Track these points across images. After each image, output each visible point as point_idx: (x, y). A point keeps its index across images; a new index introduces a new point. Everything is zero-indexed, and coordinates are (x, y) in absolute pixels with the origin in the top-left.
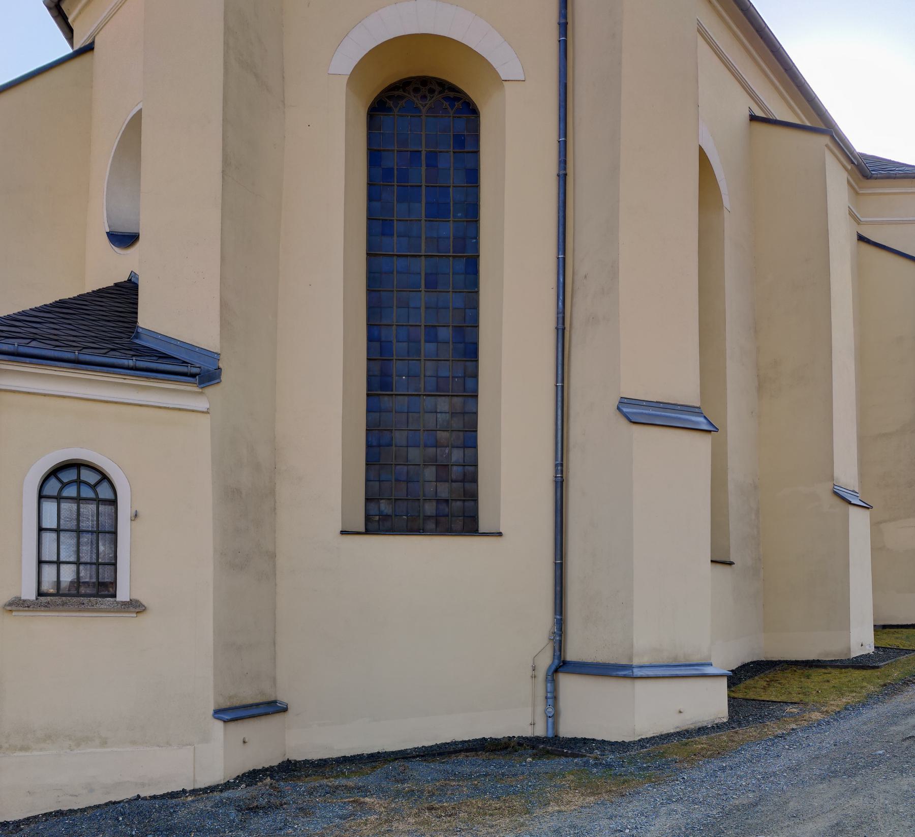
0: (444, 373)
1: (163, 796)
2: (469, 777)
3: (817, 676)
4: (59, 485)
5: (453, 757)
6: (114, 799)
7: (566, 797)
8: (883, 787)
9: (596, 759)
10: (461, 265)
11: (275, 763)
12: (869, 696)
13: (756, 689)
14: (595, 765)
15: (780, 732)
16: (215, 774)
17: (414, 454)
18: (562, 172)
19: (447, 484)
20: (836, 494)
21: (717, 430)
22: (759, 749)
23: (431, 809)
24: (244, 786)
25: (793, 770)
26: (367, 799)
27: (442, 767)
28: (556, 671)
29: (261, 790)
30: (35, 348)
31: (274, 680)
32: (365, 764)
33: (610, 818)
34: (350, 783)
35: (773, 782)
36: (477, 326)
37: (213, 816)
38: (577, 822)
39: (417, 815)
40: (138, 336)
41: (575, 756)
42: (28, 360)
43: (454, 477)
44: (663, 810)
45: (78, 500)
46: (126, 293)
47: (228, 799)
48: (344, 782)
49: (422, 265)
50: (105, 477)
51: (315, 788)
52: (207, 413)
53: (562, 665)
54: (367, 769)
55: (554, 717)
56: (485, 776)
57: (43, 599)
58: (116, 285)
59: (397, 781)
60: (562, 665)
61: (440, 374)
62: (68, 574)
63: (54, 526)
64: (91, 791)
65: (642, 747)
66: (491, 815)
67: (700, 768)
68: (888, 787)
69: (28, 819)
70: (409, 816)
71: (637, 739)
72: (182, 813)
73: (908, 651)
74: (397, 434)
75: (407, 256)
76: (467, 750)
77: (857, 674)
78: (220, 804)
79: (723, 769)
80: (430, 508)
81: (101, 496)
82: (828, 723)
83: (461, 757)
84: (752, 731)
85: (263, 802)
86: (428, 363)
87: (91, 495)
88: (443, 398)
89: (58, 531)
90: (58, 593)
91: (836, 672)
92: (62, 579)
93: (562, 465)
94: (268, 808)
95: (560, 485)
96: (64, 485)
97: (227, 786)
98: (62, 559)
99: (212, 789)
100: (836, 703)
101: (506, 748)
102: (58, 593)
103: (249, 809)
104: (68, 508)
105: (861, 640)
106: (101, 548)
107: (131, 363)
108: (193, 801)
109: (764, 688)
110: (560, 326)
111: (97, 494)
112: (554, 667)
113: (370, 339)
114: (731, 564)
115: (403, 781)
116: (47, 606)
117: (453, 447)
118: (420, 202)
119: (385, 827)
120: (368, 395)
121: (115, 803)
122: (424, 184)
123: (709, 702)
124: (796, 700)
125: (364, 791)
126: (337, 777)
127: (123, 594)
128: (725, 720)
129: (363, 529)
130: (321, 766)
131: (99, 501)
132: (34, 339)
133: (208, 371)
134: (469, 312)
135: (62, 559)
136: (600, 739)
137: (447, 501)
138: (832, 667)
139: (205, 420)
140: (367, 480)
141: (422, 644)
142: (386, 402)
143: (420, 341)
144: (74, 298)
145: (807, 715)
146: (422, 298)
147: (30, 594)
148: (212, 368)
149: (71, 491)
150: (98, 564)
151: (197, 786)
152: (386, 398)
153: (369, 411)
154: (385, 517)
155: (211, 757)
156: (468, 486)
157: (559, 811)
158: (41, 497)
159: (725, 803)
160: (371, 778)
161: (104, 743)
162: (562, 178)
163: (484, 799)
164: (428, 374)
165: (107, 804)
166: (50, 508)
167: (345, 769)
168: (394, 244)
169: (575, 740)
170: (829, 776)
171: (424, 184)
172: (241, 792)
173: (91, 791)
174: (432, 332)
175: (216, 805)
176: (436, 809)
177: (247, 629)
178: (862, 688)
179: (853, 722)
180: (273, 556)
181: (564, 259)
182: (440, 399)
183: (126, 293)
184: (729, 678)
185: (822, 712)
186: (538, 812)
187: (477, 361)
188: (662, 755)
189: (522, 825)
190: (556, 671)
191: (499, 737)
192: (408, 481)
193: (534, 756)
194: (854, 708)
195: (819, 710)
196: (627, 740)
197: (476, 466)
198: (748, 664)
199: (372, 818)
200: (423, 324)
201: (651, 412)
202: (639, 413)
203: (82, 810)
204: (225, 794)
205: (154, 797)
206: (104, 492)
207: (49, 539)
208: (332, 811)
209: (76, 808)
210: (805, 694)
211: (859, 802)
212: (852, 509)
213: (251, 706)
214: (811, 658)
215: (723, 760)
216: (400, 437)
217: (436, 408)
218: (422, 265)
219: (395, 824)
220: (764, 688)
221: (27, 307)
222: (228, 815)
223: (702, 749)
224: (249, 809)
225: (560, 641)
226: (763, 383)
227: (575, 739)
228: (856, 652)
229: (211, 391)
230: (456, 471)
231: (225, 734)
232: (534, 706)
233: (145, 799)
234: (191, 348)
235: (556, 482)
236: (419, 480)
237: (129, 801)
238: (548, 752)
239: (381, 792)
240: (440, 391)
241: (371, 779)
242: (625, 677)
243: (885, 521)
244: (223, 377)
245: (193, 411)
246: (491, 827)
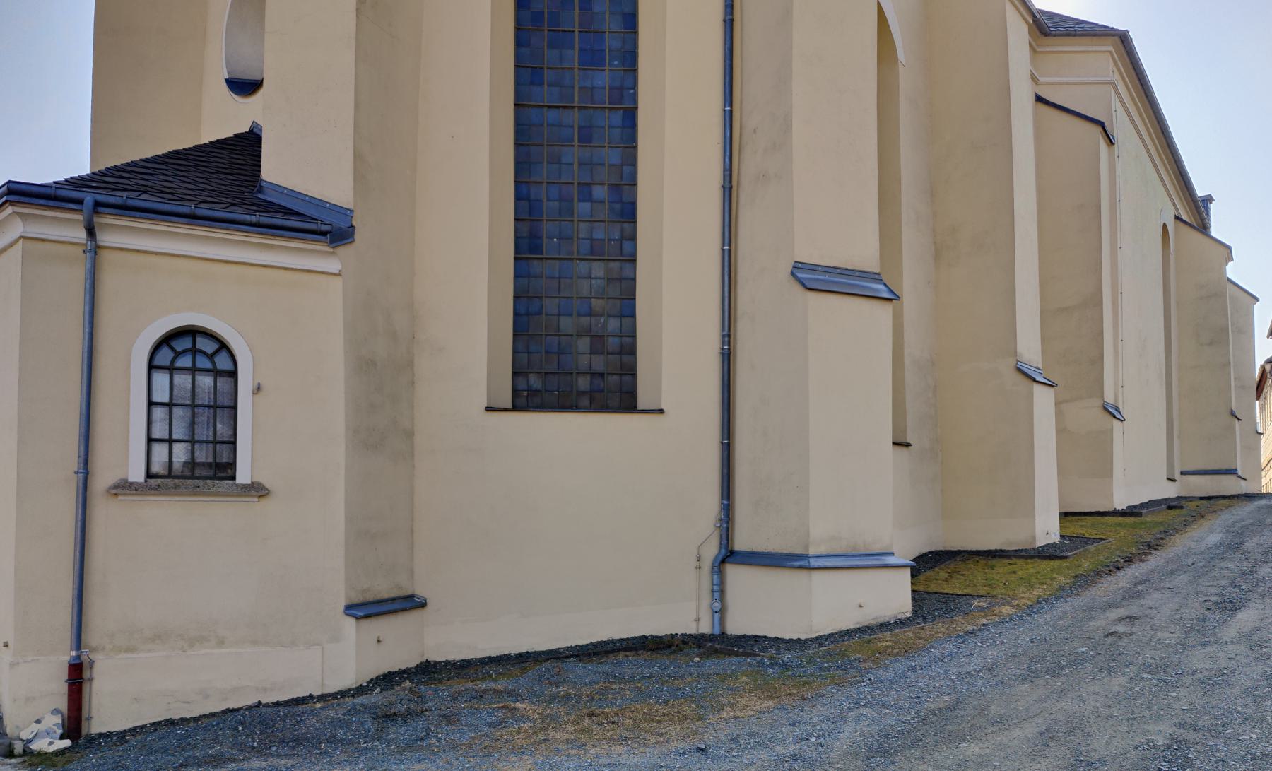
0: (599, 234)
1: (287, 703)
2: (632, 679)
3: (1002, 567)
4: (171, 355)
5: (612, 658)
6: (231, 707)
7: (745, 701)
8: (1092, 688)
9: (771, 658)
10: (617, 118)
11: (413, 664)
12: (1061, 588)
13: (938, 580)
14: (771, 665)
15: (970, 628)
16: (347, 678)
17: (566, 324)
18: (729, 17)
19: (602, 357)
20: (1019, 370)
21: (898, 298)
22: (949, 647)
23: (591, 715)
24: (378, 690)
25: (990, 670)
26: (518, 705)
27: (600, 668)
28: (723, 561)
29: (399, 695)
30: (146, 201)
31: (411, 572)
32: (513, 665)
33: (793, 724)
34: (499, 687)
35: (968, 683)
36: (636, 185)
37: (345, 725)
38: (755, 729)
39: (576, 722)
40: (261, 190)
41: (747, 655)
42: (138, 214)
43: (610, 349)
44: (851, 715)
45: (193, 370)
46: (249, 143)
47: (362, 705)
48: (492, 685)
49: (575, 118)
50: (223, 346)
51: (459, 693)
52: (339, 275)
53: (729, 556)
54: (516, 670)
55: (721, 613)
56: (649, 677)
57: (152, 482)
58: (236, 135)
59: (551, 684)
60: (729, 556)
61: (595, 236)
62: (181, 453)
63: (166, 399)
64: (207, 697)
65: (821, 645)
66: (659, 722)
67: (886, 667)
68: (1097, 689)
69: (134, 729)
70: (566, 723)
71: (814, 636)
72: (311, 721)
73: (1095, 540)
74: (547, 302)
75: (558, 107)
76: (626, 650)
77: (1045, 565)
78: (354, 711)
79: (913, 669)
80: (583, 383)
81: (220, 367)
82: (1021, 618)
83: (620, 656)
84: (940, 627)
85: (402, 708)
86: (582, 225)
87: (208, 365)
88: (598, 263)
89: (170, 405)
90: (170, 475)
91: (1021, 562)
92: (174, 459)
93: (729, 336)
94: (408, 716)
95: (727, 357)
96: (178, 354)
97: (360, 691)
98: (175, 436)
99: (342, 694)
100: (1027, 596)
101: (670, 647)
102: (170, 475)
103: (386, 716)
104: (183, 380)
105: (1047, 530)
106: (219, 426)
107: (254, 219)
108: (322, 708)
109: (946, 580)
110: (727, 185)
111: (214, 364)
112: (720, 558)
113: (518, 198)
114: (908, 445)
115: (557, 684)
116: (157, 490)
117: (609, 316)
118: (573, 48)
119: (541, 736)
120: (515, 258)
121: (233, 710)
122: (577, 29)
123: (891, 595)
124: (982, 592)
125: (514, 695)
126: (483, 679)
127: (243, 475)
128: (909, 615)
129: (510, 406)
130: (464, 668)
131: (217, 373)
132: (145, 192)
133: (340, 229)
134: (626, 169)
135: (175, 436)
136: (773, 636)
137: (602, 375)
138: (1016, 557)
139: (338, 282)
140: (515, 352)
141: (573, 532)
142: (536, 267)
143: (572, 200)
144: (190, 149)
145: (996, 610)
146: (574, 154)
147: (138, 475)
148: (344, 226)
149: (185, 361)
150: (215, 442)
151: (326, 691)
152: (535, 262)
153: (516, 276)
154: (533, 393)
155: (344, 658)
156: (626, 358)
157: (735, 718)
158: (152, 367)
159: (918, 707)
160: (522, 681)
161: (221, 643)
162: (729, 24)
163: (650, 704)
164: (581, 236)
165: (224, 712)
166: (161, 379)
167: (492, 670)
168: (545, 94)
169: (744, 638)
170: (1031, 675)
171: (577, 29)
172: (375, 698)
173: (207, 697)
174: (586, 191)
175: (349, 713)
176: (597, 715)
177: (378, 521)
178: (1052, 579)
179: (1048, 617)
180: (410, 434)
181: (731, 111)
182: (595, 264)
183: (249, 143)
184: (912, 568)
185: (1013, 606)
186: (712, 718)
187: (635, 222)
188: (843, 654)
189: (696, 733)
190: (723, 561)
191: (661, 634)
192: (559, 353)
193: (701, 656)
194: (1047, 601)
195: (1009, 604)
196: (803, 637)
197: (634, 336)
198: (926, 554)
199: (526, 726)
200: (576, 182)
201: (827, 277)
202: (815, 279)
203: (196, 719)
204: (359, 700)
205: (277, 704)
206: (222, 362)
207: (159, 413)
208: (480, 719)
209: (188, 716)
210: (991, 586)
211: (1067, 704)
212: (1037, 387)
213: (386, 601)
214: (993, 548)
215: (912, 658)
216: (550, 305)
217: (590, 273)
218: (575, 118)
219: (552, 733)
220: (946, 580)
221: (136, 158)
222: (362, 724)
223: (887, 647)
224: (386, 716)
225: (728, 529)
226: (939, 252)
227: (744, 636)
228: (1041, 542)
229: (343, 251)
230: (613, 343)
231: (358, 631)
232: (699, 599)
233: (267, 705)
234: (320, 204)
235: (723, 355)
236: (571, 354)
237: (250, 708)
238: (716, 651)
239: (535, 696)
240: (595, 252)
241: (523, 682)
242: (800, 567)
243: (1067, 401)
244: (357, 236)
245: (323, 273)
246: (661, 735)
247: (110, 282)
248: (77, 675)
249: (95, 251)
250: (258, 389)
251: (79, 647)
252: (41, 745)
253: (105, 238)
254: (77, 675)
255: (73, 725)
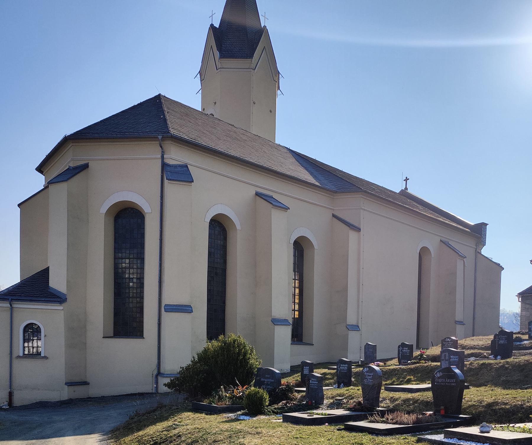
116: (25, 357)
127: (42, 355)
129: (112, 335)
147: (21, 354)
202: (185, 309)
247: (15, 315)
248: (11, 394)
249: (12, 308)
250: (45, 336)
251: (11, 389)
252: (4, 407)
253: (14, 306)
254: (11, 394)
255: (10, 403)
